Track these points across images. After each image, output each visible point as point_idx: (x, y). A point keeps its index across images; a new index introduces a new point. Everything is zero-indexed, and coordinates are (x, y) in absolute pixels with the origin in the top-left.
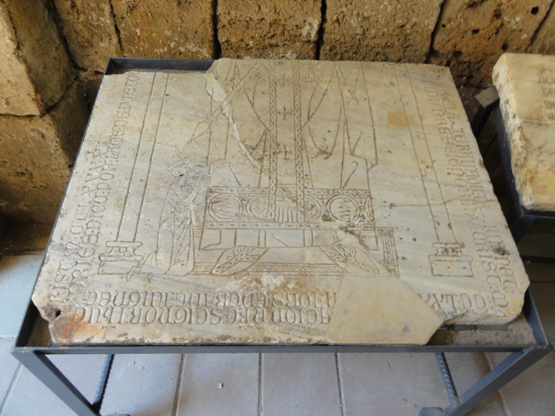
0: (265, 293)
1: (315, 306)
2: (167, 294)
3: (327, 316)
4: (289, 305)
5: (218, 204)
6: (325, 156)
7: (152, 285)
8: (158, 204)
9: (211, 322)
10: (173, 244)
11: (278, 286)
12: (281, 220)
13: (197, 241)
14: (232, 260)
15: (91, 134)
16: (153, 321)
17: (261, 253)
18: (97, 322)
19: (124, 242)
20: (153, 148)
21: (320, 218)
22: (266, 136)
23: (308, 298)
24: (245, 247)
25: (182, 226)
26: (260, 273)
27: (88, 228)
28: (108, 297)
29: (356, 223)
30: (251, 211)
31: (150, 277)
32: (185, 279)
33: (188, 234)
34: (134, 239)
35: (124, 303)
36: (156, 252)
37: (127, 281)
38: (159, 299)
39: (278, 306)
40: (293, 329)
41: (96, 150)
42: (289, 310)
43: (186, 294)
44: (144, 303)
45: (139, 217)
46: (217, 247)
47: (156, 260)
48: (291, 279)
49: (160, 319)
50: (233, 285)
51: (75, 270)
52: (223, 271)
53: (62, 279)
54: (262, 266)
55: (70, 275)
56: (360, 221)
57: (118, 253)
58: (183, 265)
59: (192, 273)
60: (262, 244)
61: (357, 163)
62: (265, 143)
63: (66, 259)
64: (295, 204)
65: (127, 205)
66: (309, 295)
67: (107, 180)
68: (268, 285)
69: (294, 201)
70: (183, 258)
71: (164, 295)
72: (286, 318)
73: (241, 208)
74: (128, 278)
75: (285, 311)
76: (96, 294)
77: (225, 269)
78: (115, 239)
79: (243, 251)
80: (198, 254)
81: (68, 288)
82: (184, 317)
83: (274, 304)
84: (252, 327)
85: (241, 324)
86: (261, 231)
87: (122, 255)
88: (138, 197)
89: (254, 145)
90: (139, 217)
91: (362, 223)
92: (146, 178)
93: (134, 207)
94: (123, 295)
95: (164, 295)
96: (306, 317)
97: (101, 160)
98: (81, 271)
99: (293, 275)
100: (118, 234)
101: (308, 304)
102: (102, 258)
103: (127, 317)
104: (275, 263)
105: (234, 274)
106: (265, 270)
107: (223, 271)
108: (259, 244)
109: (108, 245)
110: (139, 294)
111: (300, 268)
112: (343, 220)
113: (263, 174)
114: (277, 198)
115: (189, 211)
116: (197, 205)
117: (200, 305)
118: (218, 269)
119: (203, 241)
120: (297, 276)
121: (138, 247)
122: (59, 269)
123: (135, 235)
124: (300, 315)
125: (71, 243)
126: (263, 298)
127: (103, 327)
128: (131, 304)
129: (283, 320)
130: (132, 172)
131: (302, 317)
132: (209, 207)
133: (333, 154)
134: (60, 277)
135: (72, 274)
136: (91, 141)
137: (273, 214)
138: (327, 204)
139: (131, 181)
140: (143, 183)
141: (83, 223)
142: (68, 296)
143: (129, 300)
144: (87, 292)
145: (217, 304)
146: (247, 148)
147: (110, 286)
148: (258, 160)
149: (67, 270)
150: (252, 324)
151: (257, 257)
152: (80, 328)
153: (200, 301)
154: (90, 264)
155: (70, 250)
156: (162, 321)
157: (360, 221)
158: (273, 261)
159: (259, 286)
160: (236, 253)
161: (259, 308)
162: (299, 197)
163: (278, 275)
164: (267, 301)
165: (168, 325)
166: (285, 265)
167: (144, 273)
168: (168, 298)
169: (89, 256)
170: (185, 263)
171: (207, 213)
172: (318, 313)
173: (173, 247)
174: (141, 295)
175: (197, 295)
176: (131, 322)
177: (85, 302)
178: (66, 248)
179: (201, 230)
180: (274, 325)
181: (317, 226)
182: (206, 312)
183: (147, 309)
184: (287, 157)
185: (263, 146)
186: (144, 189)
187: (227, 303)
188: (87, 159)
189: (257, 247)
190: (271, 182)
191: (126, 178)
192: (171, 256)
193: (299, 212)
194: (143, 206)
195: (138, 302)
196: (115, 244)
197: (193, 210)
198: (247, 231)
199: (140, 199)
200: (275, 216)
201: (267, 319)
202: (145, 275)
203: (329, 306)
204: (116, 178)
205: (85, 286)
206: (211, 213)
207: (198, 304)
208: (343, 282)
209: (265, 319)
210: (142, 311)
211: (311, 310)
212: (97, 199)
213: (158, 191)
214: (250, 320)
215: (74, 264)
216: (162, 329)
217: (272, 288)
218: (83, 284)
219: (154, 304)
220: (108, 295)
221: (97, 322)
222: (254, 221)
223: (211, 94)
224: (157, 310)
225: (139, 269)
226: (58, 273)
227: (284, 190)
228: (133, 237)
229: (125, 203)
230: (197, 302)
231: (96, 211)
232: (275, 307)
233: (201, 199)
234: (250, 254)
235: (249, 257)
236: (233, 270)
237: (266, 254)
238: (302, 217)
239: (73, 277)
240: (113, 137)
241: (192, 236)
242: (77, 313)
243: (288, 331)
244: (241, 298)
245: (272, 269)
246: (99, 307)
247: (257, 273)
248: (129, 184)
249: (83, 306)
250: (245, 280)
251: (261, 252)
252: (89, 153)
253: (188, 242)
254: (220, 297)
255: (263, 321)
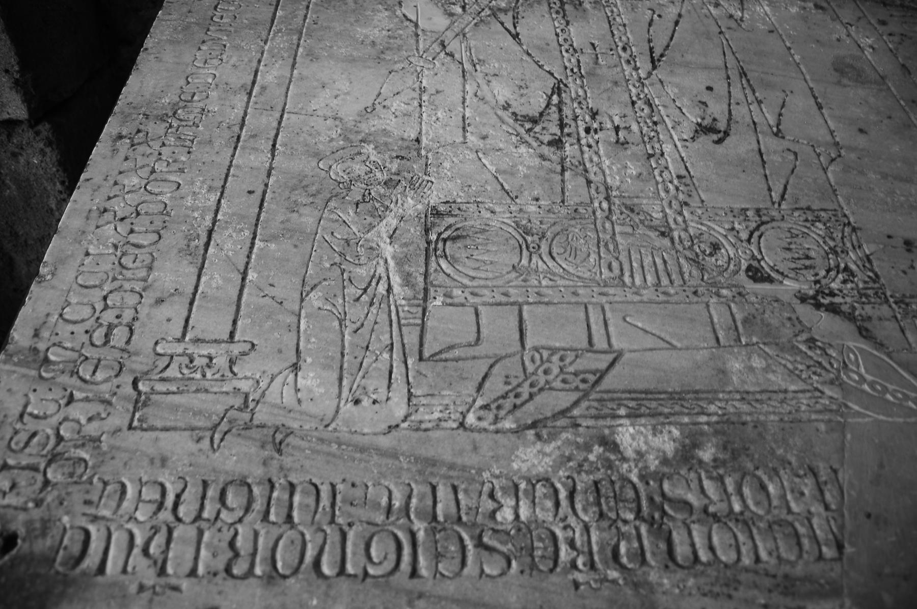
0: (635, 479)
1: (789, 511)
2: (333, 486)
3: (831, 536)
4: (711, 509)
5: (459, 244)
6: (715, 137)
7: (287, 461)
8: (296, 246)
9: (482, 571)
10: (343, 346)
11: (670, 454)
12: (638, 281)
13: (411, 338)
14: (519, 385)
15: (130, 100)
16: (296, 571)
17: (603, 366)
18: (124, 571)
19: (204, 341)
20: (280, 123)
21: (742, 273)
22: (559, 95)
23: (763, 488)
24: (553, 351)
25: (365, 298)
26: (609, 422)
27: (106, 307)
28: (157, 496)
29: (834, 285)
30: (553, 258)
31: (279, 437)
32: (385, 442)
33: (383, 317)
34: (232, 334)
35: (205, 515)
36: (296, 368)
37: (214, 451)
38: (311, 501)
39: (679, 516)
40: (739, 582)
41: (139, 131)
42: (715, 526)
43: (392, 487)
44: (267, 513)
45: (244, 279)
46: (471, 352)
47: (297, 390)
48: (702, 434)
49: (317, 564)
50: (532, 458)
51: (66, 419)
52: (496, 420)
53: (27, 444)
54: (613, 400)
55: (49, 431)
56: (844, 282)
57: (185, 371)
58: (375, 402)
59: (405, 425)
60: (600, 342)
61: (796, 154)
62: (560, 110)
63: (42, 388)
64: (666, 242)
65: (211, 250)
66: (765, 478)
67: (160, 193)
68: (640, 454)
69: (663, 234)
70: (375, 383)
71: (325, 491)
72: (711, 548)
73: (525, 252)
74: (216, 441)
75: (706, 530)
76: (123, 486)
77: (502, 413)
78: (179, 334)
79: (549, 361)
80: (419, 373)
81: (42, 467)
82: (392, 557)
83: (666, 507)
84: (614, 582)
85: (580, 577)
86: (590, 308)
87: (198, 376)
88: (241, 230)
89: (534, 112)
90: (244, 279)
91: (849, 286)
92: (262, 187)
93: (230, 253)
94: (201, 489)
95: (325, 491)
96: (770, 545)
97: (149, 151)
98: (83, 421)
99: (708, 423)
100: (187, 321)
101: (766, 503)
102: (141, 386)
103: (214, 555)
104: (646, 392)
105: (534, 425)
106: (622, 412)
107: (496, 420)
108: (590, 342)
109: (159, 349)
110: (249, 486)
111: (723, 405)
112: (801, 278)
113: (567, 174)
114: (618, 229)
115: (382, 262)
116: (406, 245)
117: (441, 518)
118: (482, 413)
119: (428, 337)
120: (718, 427)
121: (244, 354)
122: (21, 416)
123: (235, 322)
124: (752, 538)
125: (59, 345)
126: (630, 494)
127: (141, 588)
128: (224, 515)
129: (704, 556)
130: (227, 176)
131: (760, 544)
132: (435, 250)
133: (731, 132)
134: (23, 437)
135: (58, 430)
136: (130, 114)
137: (615, 265)
138: (749, 241)
139: (222, 193)
140: (256, 198)
141: (96, 296)
142: (41, 491)
143: (219, 506)
144: (95, 480)
145: (492, 515)
146: (516, 120)
147: (164, 461)
148: (550, 144)
149: (45, 417)
150: (613, 574)
151: (592, 378)
152: (71, 590)
153: (440, 507)
154: (109, 403)
155: (54, 363)
156: (326, 570)
157: (844, 282)
158: (641, 386)
159: (613, 457)
160: (530, 368)
161: (625, 522)
162: (673, 226)
163: (663, 424)
164: (644, 503)
165: (344, 585)
166: (676, 397)
167: (262, 426)
168: (339, 497)
169: (106, 380)
170: (382, 394)
171: (433, 265)
172: (802, 530)
173: (343, 355)
174: (256, 490)
175: (428, 490)
176: (228, 570)
177: (91, 511)
178: (46, 360)
179: (420, 309)
180: (680, 574)
181: (740, 294)
182: (461, 540)
183: (275, 531)
184: (622, 139)
185: (556, 116)
186: (257, 210)
187: (524, 513)
188: (115, 151)
189: (588, 351)
190: (593, 191)
191: (210, 189)
192: (341, 379)
193: (682, 261)
194: (255, 250)
195: (247, 510)
196: (179, 349)
197: (394, 257)
198: (551, 308)
199: (247, 234)
200: (622, 270)
201: (653, 554)
202: (265, 431)
203: (827, 508)
204: (182, 191)
205: (90, 464)
206: (444, 264)
207: (435, 517)
208: (849, 436)
209: (648, 556)
210: (261, 540)
211: (780, 523)
212: (133, 239)
213: (295, 215)
214: (605, 563)
215: (63, 402)
216: (327, 595)
217: (653, 463)
218: (86, 456)
219: (295, 514)
220: (158, 489)
221: (124, 571)
222: (567, 283)
223: (414, 18)
224: (308, 537)
225: (246, 416)
226: (19, 426)
227: (632, 211)
228: (229, 327)
229: (207, 245)
230: (430, 509)
231: (130, 265)
232: (672, 518)
233: (414, 231)
234: (571, 369)
235: (570, 378)
236: (529, 412)
237: (618, 367)
238: (695, 272)
239: (60, 439)
240: (181, 104)
241: (395, 325)
242: (66, 542)
243: (725, 590)
244: (563, 494)
245: (643, 409)
246: (129, 526)
247: (601, 422)
248: (219, 201)
249: (83, 522)
250: (568, 442)
251: (602, 362)
252: (120, 137)
253: (386, 339)
254: (499, 494)
255: (644, 562)
